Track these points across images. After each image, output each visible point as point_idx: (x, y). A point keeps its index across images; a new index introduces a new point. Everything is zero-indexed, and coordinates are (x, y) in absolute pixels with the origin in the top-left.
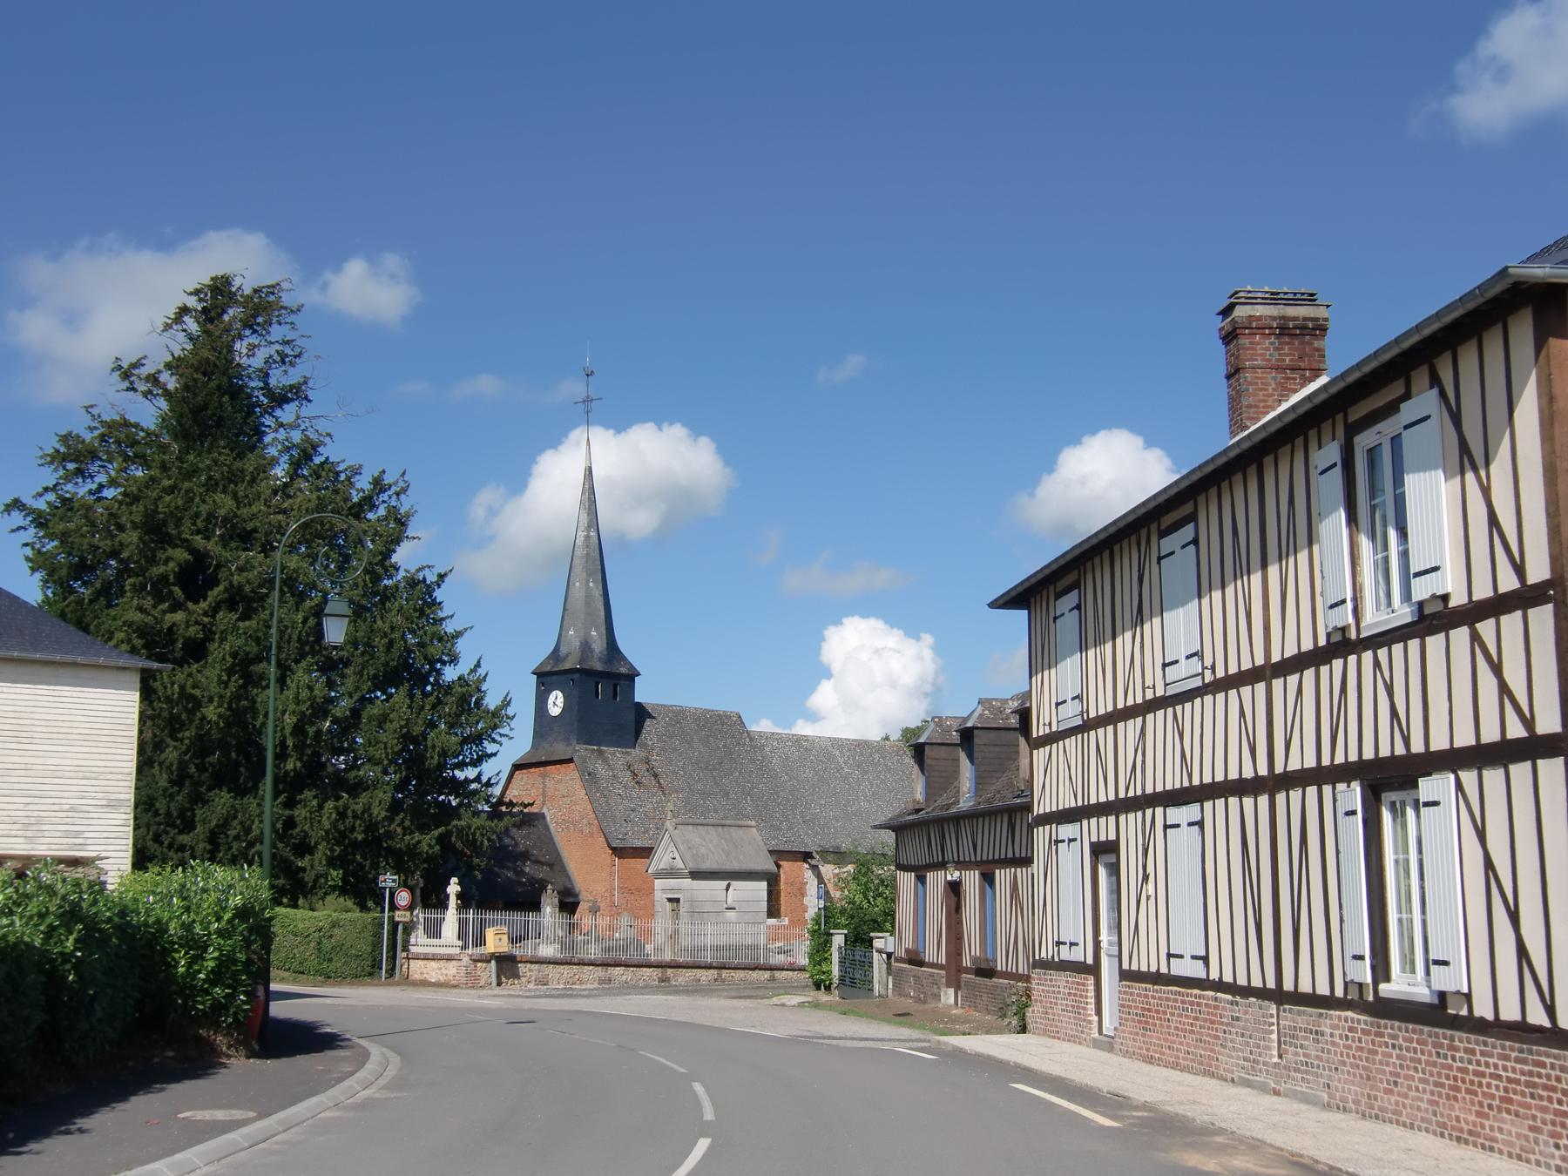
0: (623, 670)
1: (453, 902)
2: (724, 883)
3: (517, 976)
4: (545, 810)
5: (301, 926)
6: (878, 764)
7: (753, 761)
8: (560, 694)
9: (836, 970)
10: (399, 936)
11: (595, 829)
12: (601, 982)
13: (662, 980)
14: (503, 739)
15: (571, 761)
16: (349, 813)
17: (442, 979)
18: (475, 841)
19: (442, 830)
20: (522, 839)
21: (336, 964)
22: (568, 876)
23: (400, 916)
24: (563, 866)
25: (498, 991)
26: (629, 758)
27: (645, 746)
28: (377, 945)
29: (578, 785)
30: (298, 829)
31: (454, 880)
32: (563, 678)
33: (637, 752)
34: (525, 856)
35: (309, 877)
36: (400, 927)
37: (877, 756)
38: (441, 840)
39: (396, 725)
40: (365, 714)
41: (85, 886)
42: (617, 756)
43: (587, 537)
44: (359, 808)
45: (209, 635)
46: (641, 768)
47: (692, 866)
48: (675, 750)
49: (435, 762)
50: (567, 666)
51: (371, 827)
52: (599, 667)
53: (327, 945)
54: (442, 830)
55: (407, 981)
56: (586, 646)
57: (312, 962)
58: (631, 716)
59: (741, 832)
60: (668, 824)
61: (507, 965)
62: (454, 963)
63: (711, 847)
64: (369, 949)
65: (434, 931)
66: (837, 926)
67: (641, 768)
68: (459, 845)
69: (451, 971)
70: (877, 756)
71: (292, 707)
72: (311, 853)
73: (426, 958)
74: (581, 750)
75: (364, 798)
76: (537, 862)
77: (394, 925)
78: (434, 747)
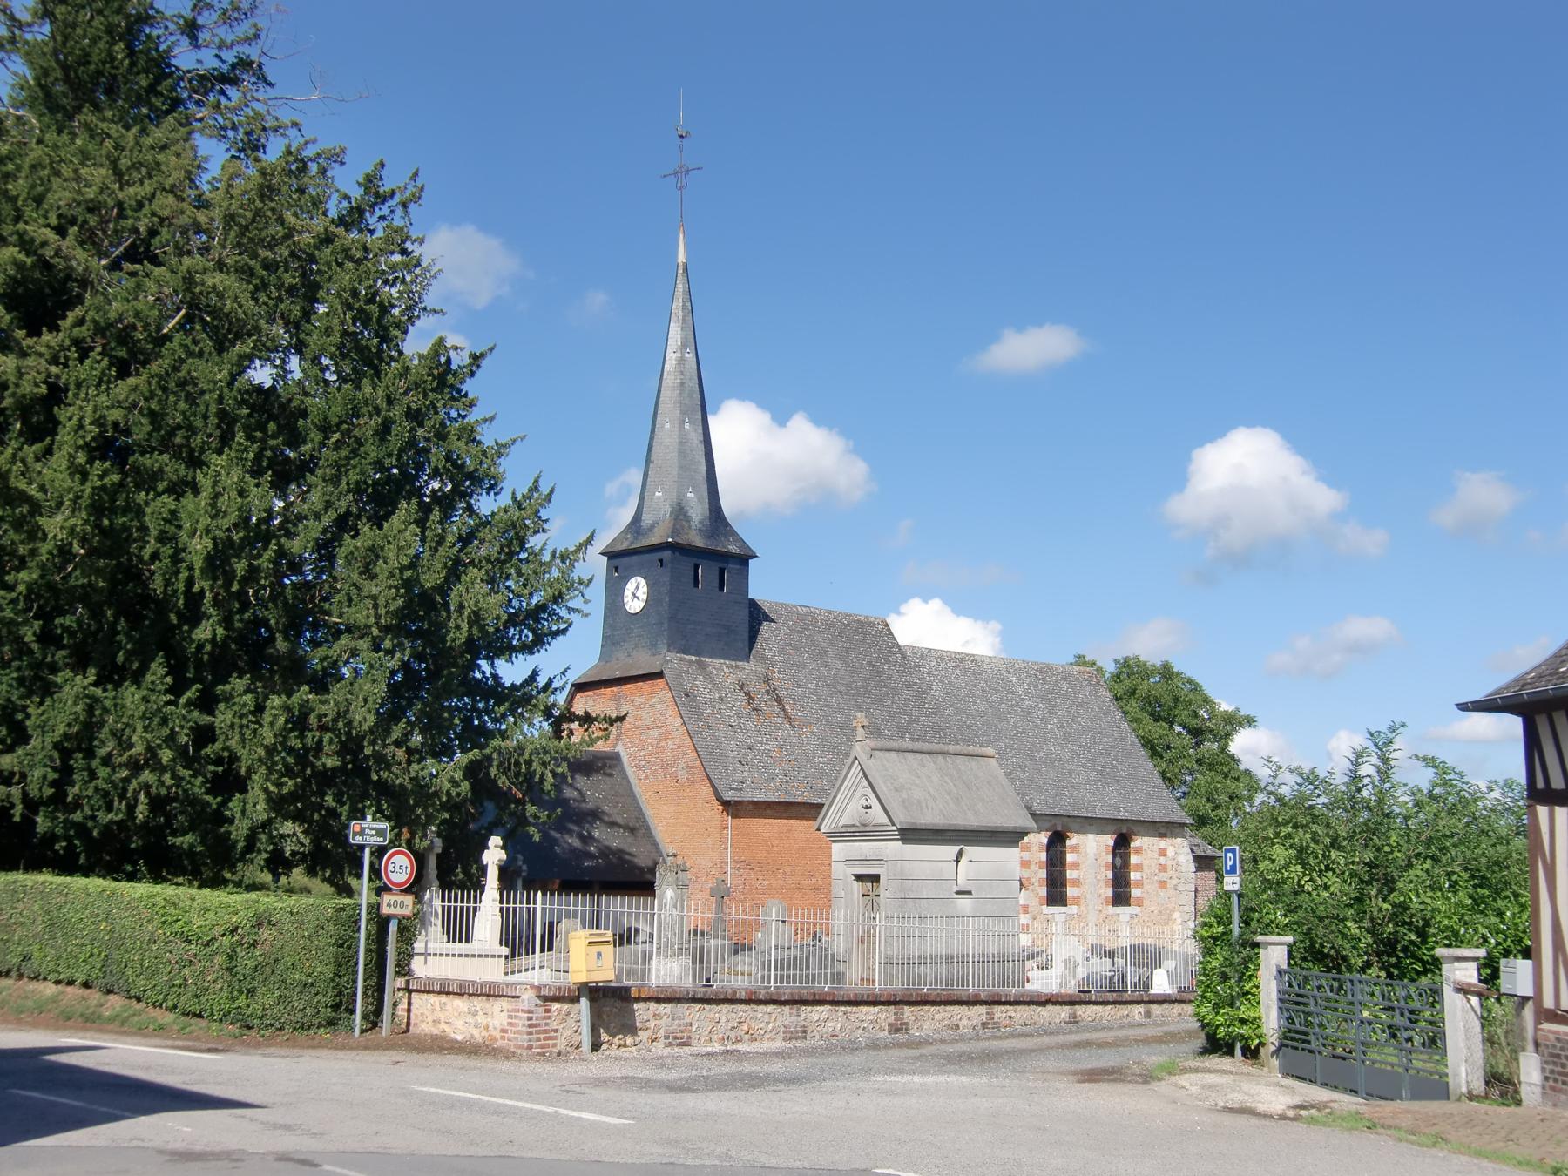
0: (733, 549)
1: (492, 880)
2: (951, 851)
3: (631, 1029)
4: (619, 748)
5: (197, 922)
6: (1066, 696)
7: (908, 685)
8: (642, 582)
9: (1271, 1021)
10: (387, 947)
11: (698, 774)
12: (790, 1035)
13: (896, 1029)
14: (574, 617)
15: (659, 675)
16: (312, 720)
17: (478, 1035)
18: (530, 776)
19: (475, 754)
20: (590, 790)
21: (265, 999)
22: (656, 845)
23: (397, 905)
24: (648, 829)
25: (595, 1066)
26: (742, 675)
27: (763, 658)
28: (344, 962)
29: (670, 711)
30: (218, 746)
31: (495, 841)
32: (647, 557)
33: (752, 667)
34: (595, 815)
35: (239, 831)
36: (393, 927)
37: (1064, 685)
38: (472, 771)
39: (393, 564)
40: (342, 552)
41: (1245, 1012)
42: (725, 671)
43: (681, 360)
44: (329, 710)
45: (56, 394)
46: (758, 689)
47: (902, 819)
48: (804, 666)
49: (462, 636)
50: (654, 539)
51: (350, 745)
52: (699, 542)
53: (245, 963)
54: (475, 754)
55: (408, 1041)
56: (680, 513)
57: (217, 997)
58: (743, 615)
59: (973, 764)
60: (858, 749)
61: (611, 1005)
62: (504, 1003)
63: (927, 789)
64: (329, 972)
65: (459, 929)
66: (1267, 928)
67: (758, 689)
68: (503, 782)
69: (494, 1019)
70: (1064, 685)
71: (205, 521)
72: (244, 791)
73: (445, 990)
74: (673, 662)
75: (337, 692)
76: (613, 824)
77: (382, 923)
78: (461, 607)
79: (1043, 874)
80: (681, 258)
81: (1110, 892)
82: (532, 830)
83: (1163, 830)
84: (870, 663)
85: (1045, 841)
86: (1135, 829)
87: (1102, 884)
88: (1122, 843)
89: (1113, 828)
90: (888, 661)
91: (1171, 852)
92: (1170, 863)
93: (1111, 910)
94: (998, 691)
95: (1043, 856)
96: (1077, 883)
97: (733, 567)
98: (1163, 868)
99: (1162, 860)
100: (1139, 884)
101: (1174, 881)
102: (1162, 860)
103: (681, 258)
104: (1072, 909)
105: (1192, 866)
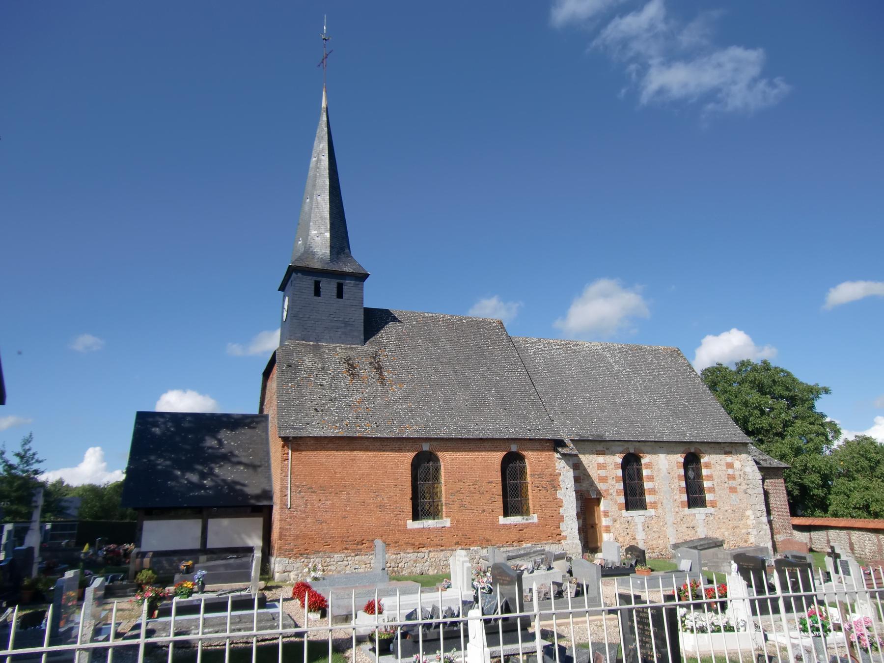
26: (351, 353)
27: (378, 343)
70: (650, 358)
79: (621, 486)
80: (324, 105)
81: (685, 498)
82: (816, 492)
83: (727, 449)
84: (477, 345)
85: (620, 461)
86: (703, 448)
87: (677, 492)
88: (692, 461)
89: (682, 449)
90: (494, 343)
91: (737, 465)
92: (737, 473)
93: (687, 511)
94: (593, 362)
95: (620, 472)
96: (653, 491)
97: (349, 285)
98: (732, 477)
99: (730, 471)
100: (712, 490)
101: (744, 487)
102: (730, 471)
103: (324, 105)
104: (651, 512)
105: (758, 476)
